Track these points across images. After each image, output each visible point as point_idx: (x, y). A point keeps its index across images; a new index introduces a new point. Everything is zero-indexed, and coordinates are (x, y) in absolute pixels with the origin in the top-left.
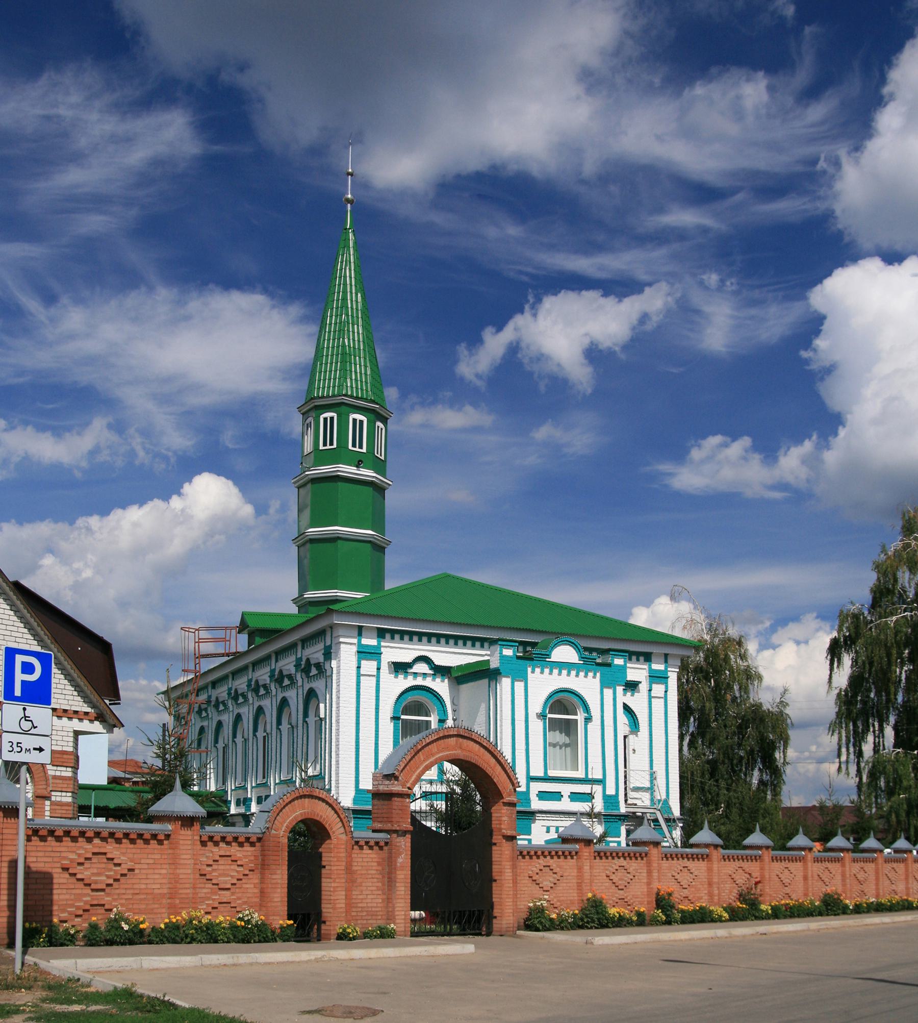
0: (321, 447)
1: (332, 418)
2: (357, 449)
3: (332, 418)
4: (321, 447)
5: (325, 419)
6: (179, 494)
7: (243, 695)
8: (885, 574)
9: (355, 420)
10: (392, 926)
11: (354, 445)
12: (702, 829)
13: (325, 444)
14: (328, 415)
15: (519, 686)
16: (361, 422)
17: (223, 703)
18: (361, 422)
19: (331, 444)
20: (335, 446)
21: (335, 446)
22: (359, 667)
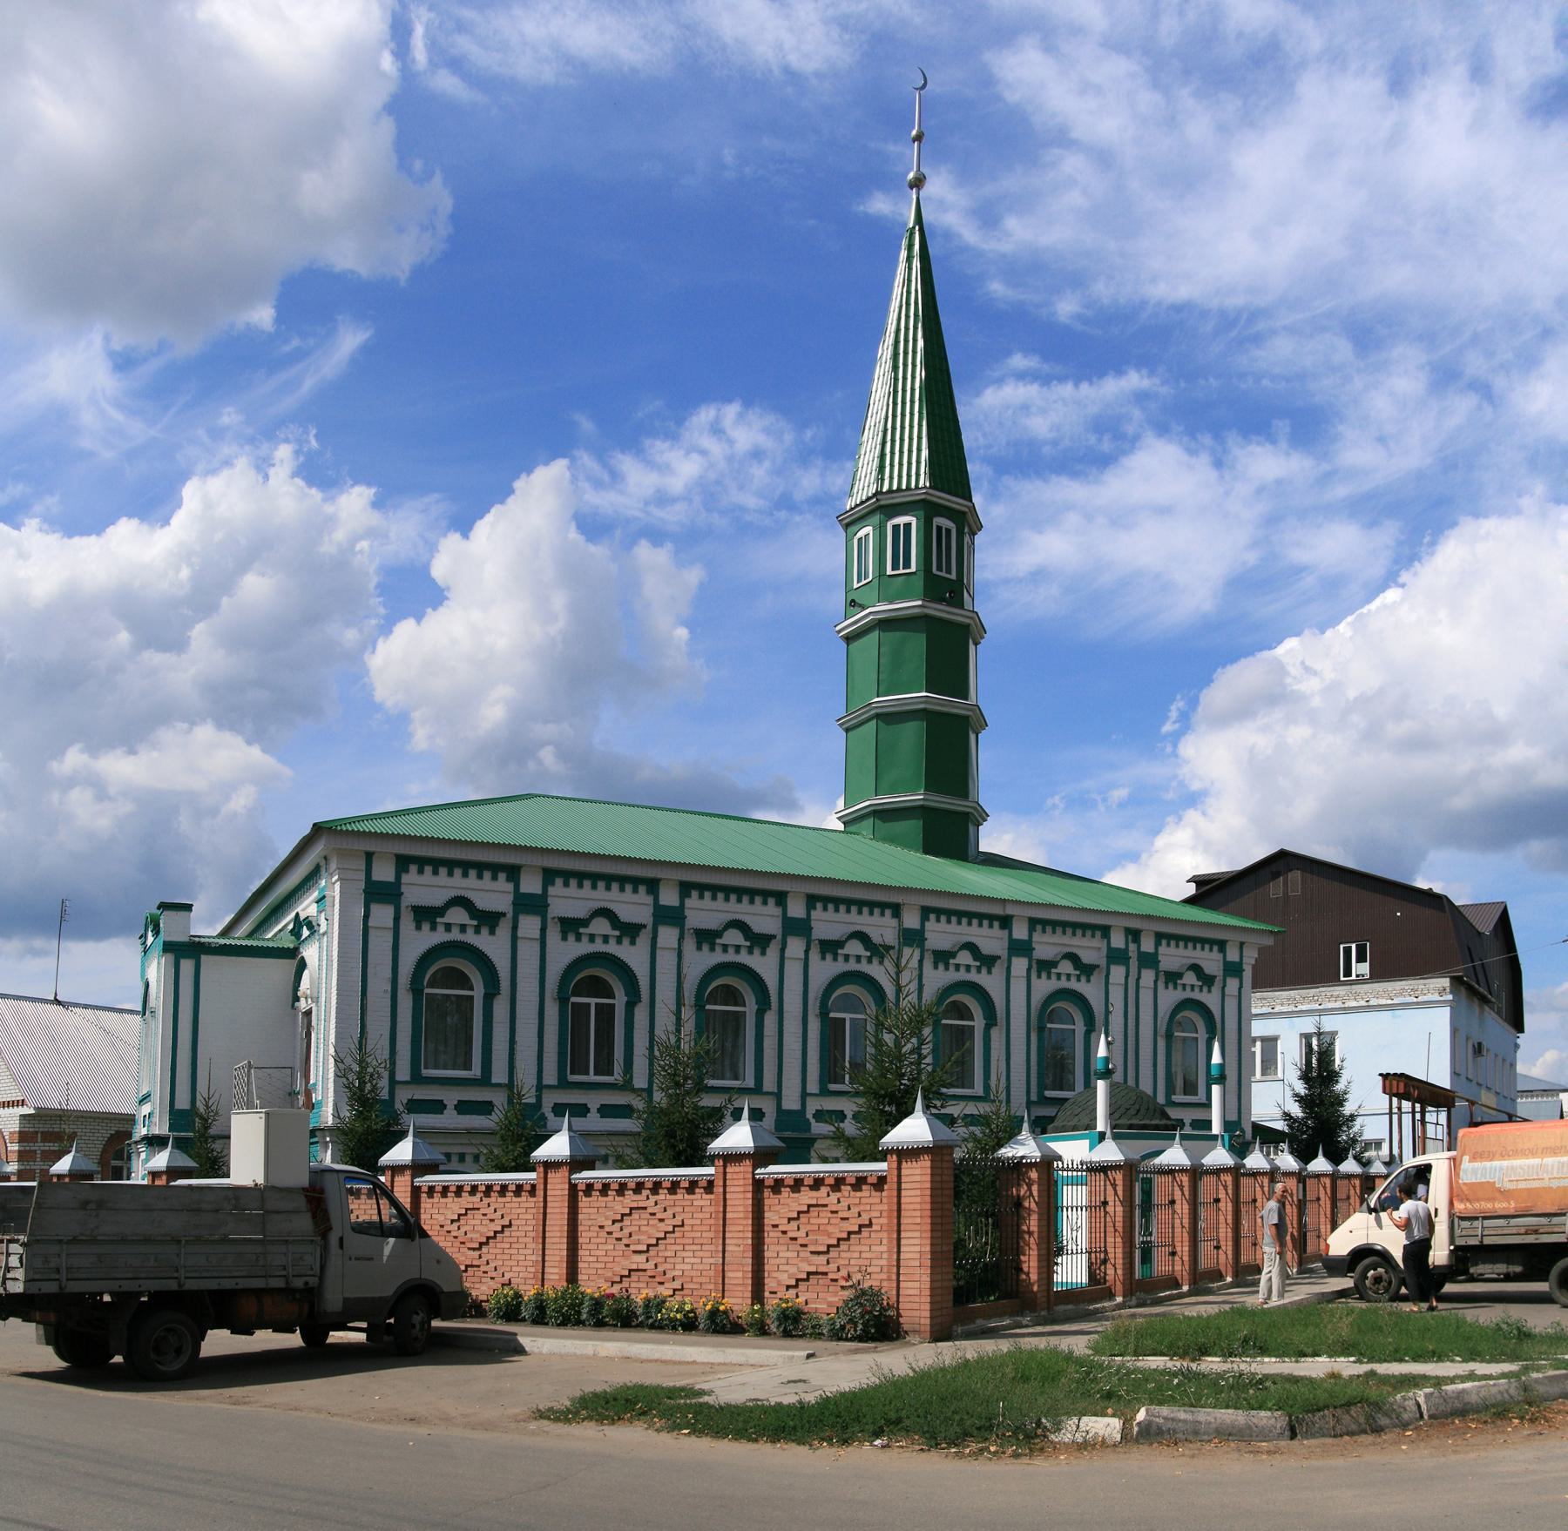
0: (889, 572)
1: (908, 526)
2: (943, 574)
3: (908, 526)
4: (889, 572)
5: (896, 528)
6: (419, 620)
7: (310, 926)
8: (229, 365)
9: (939, 528)
10: (496, 1152)
11: (939, 568)
12: (912, 1112)
13: (895, 566)
14: (901, 520)
15: (183, 1103)
16: (948, 531)
17: (310, 926)
18: (948, 531)
19: (907, 565)
20: (913, 569)
21: (913, 569)
22: (366, 917)
